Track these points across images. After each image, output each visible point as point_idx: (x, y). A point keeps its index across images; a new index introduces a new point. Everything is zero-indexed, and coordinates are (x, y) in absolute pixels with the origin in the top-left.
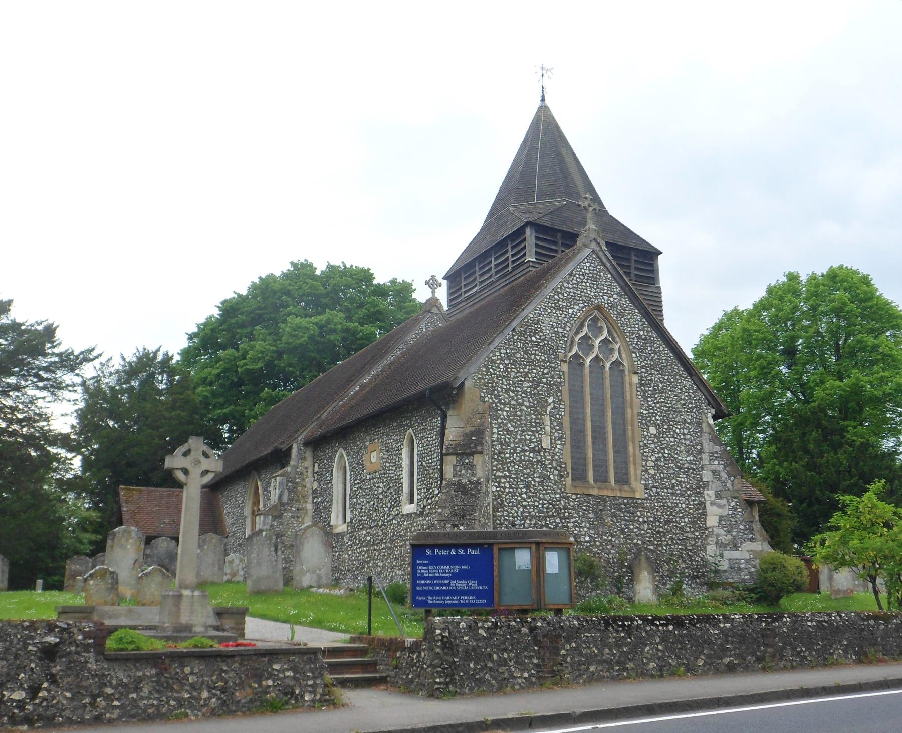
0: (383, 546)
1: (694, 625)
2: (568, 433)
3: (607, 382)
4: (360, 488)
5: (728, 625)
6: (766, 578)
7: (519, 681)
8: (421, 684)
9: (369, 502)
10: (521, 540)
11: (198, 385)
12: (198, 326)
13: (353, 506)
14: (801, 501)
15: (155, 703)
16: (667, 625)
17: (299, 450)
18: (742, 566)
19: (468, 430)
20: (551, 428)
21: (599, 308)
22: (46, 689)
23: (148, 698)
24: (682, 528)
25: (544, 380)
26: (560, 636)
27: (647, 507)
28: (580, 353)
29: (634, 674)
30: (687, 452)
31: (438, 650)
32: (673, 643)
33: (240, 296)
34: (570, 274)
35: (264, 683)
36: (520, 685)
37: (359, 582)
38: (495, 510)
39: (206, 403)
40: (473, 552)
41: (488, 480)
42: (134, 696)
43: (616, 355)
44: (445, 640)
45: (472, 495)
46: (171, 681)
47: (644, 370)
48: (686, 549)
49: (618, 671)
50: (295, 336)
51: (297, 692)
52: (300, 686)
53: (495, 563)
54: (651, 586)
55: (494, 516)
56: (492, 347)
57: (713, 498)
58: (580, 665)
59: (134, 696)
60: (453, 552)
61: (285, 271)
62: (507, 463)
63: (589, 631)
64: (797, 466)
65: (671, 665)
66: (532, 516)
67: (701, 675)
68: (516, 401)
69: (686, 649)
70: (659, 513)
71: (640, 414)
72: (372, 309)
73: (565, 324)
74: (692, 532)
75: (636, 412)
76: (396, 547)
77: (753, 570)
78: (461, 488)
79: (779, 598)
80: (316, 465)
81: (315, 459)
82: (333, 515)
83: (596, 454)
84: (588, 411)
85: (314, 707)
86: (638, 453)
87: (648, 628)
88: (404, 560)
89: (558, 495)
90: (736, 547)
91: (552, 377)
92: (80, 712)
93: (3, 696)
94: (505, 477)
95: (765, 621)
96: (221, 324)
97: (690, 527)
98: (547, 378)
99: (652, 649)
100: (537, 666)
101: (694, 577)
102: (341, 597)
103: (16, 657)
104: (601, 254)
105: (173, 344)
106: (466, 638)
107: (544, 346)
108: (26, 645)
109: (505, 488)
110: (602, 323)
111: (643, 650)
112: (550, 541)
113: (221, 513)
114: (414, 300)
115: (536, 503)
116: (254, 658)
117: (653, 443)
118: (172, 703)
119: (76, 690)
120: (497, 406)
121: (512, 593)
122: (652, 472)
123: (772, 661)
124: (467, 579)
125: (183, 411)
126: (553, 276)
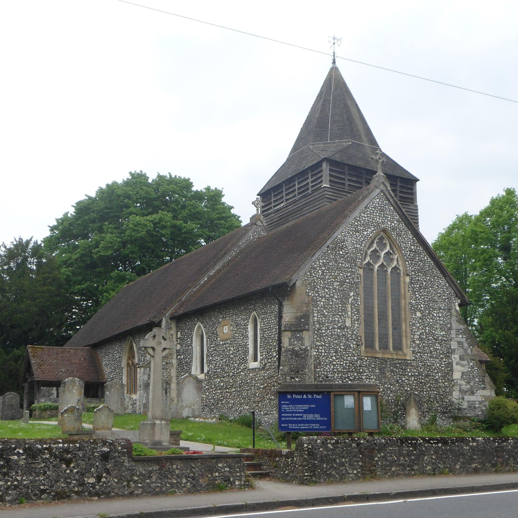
0: (233, 389)
1: (454, 444)
2: (363, 316)
3: (389, 282)
4: (215, 350)
5: (475, 444)
6: (493, 414)
7: (352, 475)
8: (295, 477)
9: (222, 360)
10: (346, 390)
11: (60, 266)
12: (57, 220)
13: (209, 362)
14: (511, 358)
15: (159, 485)
16: (437, 443)
17: (167, 322)
18: (477, 406)
19: (298, 315)
20: (352, 313)
21: (384, 231)
22: (105, 477)
23: (156, 482)
24: (436, 380)
25: (348, 281)
26: (374, 449)
27: (414, 366)
28: (371, 262)
29: (418, 473)
30: (441, 329)
31: (306, 456)
32: (441, 455)
33: (90, 198)
34: (366, 208)
35: (214, 474)
36: (352, 478)
37: (215, 414)
38: (315, 367)
39: (68, 280)
40: (317, 397)
41: (311, 348)
42: (148, 481)
43: (395, 263)
44: (310, 450)
45: (303, 358)
46: (166, 473)
47: (413, 273)
48: (439, 394)
49: (408, 470)
50: (136, 230)
51: (232, 480)
52: (233, 476)
53: (332, 404)
54: (417, 419)
55: (315, 371)
56: (314, 258)
57: (458, 360)
58: (386, 467)
59: (148, 481)
60: (305, 397)
61: (125, 180)
62: (323, 336)
63: (391, 446)
64: (509, 333)
65: (440, 468)
66: (339, 371)
67: (458, 474)
68: (329, 295)
69: (449, 458)
70: (422, 370)
71: (410, 303)
72: (193, 211)
73: (362, 242)
74: (444, 383)
75: (407, 302)
76: (244, 390)
77: (484, 408)
78: (295, 354)
79: (502, 427)
80: (179, 333)
81: (178, 328)
82: (193, 368)
83: (382, 329)
84: (376, 301)
85: (241, 488)
86: (408, 329)
87: (426, 445)
88: (250, 400)
89: (356, 358)
90: (473, 393)
91: (353, 279)
92: (122, 490)
93: (85, 481)
94: (322, 346)
95: (498, 442)
96: (77, 220)
97: (442, 380)
98: (349, 279)
99: (428, 458)
100: (362, 466)
101: (444, 413)
102: (214, 424)
103: (89, 459)
104: (386, 193)
105: (39, 232)
106: (321, 449)
107: (347, 257)
108: (93, 453)
109: (322, 353)
110: (386, 241)
111: (423, 458)
112: (366, 390)
113: (100, 365)
114: (223, 204)
115: (342, 363)
116: (208, 460)
117: (419, 322)
118: (168, 485)
119: (119, 478)
120: (317, 298)
121: (342, 423)
122: (418, 342)
123: (502, 466)
124: (313, 413)
125: (52, 286)
126: (355, 209)
